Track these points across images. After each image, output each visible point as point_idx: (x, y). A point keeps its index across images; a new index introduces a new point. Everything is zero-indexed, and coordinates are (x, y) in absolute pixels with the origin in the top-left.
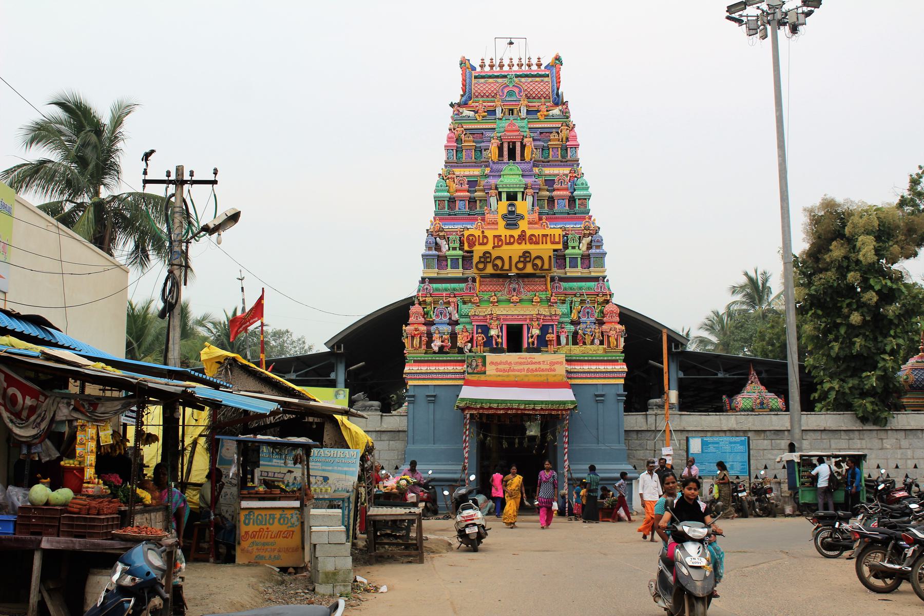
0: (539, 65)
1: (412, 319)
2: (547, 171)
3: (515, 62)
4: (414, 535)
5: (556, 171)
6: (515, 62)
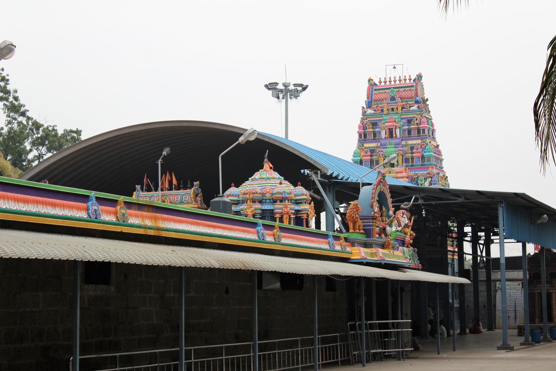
0: (410, 80)
2: (410, 142)
3: (397, 79)
4: (495, 252)
5: (415, 142)
6: (397, 79)
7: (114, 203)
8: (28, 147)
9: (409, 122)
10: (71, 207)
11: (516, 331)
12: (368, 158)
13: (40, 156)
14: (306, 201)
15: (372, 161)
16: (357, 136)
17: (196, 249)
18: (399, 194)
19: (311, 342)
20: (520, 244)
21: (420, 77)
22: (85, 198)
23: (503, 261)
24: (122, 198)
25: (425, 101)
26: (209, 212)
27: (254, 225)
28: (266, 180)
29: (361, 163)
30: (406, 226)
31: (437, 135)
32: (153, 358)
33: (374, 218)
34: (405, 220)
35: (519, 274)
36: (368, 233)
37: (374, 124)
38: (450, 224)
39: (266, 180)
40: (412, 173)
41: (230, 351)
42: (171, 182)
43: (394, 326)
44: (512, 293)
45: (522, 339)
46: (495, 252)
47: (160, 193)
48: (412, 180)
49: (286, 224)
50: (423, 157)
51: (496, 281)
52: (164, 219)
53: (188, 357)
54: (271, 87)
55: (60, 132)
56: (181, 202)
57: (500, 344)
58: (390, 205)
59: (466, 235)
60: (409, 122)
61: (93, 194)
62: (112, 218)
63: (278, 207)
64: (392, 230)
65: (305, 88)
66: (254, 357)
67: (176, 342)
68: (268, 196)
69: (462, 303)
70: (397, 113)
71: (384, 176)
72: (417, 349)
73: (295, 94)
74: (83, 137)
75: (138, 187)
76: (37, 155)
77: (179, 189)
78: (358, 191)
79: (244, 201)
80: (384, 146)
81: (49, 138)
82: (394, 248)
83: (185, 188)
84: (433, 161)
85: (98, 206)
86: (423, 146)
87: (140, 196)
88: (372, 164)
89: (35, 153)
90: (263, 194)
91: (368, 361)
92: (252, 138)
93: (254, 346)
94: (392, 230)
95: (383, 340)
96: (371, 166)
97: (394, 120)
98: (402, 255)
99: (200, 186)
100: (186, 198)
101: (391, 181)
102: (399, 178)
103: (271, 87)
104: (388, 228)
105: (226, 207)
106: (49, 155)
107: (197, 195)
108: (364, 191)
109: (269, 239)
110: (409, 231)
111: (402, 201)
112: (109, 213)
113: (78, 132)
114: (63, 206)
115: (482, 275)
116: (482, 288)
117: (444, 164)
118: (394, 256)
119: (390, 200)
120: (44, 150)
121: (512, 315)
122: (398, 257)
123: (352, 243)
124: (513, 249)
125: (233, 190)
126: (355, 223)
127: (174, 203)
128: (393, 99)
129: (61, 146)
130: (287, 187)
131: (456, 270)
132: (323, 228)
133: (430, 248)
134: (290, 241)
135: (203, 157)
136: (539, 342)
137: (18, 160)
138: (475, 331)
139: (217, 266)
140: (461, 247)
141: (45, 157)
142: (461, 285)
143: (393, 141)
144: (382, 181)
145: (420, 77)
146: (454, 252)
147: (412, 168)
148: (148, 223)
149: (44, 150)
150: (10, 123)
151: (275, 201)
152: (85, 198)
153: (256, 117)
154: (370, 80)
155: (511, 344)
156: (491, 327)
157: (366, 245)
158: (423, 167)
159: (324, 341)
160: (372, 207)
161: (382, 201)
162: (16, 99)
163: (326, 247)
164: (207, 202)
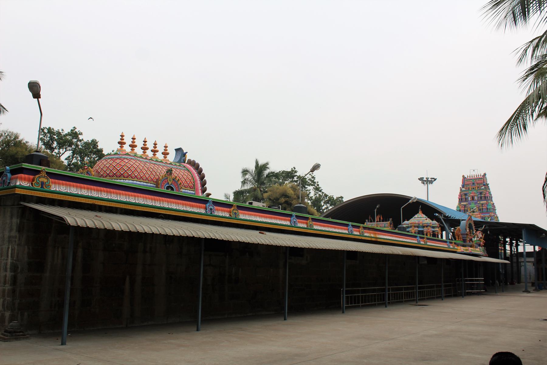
4: (521, 249)
7: (359, 227)
8: (323, 204)
9: (481, 193)
10: (342, 229)
11: (530, 284)
12: (463, 209)
13: (327, 208)
14: (437, 227)
15: (465, 210)
16: (458, 200)
17: (267, 233)
18: (478, 224)
19: (440, 286)
20: (532, 247)
21: (485, 174)
22: (347, 225)
23: (525, 254)
24: (362, 225)
25: (487, 185)
26: (396, 231)
27: (416, 237)
28: (420, 218)
29: (460, 211)
30: (481, 238)
31: (493, 199)
32: (374, 291)
33: (467, 234)
34: (480, 236)
35: (532, 259)
36: (464, 241)
37: (466, 195)
38: (500, 237)
39: (420, 218)
40: (482, 215)
41: (406, 289)
42: (380, 218)
43: (476, 281)
44: (529, 268)
45: (534, 288)
46: (521, 249)
47: (376, 223)
48: (482, 218)
49: (428, 237)
50: (487, 209)
51: (521, 262)
52: (379, 234)
53: (389, 291)
54: (421, 179)
55: (335, 198)
56: (384, 227)
57: (524, 290)
58: (474, 229)
59: (507, 242)
60: (481, 193)
61: (350, 223)
62: (358, 233)
63: (425, 229)
64: (475, 239)
65: (435, 180)
66: (416, 292)
67: (384, 284)
68: (421, 225)
69: (506, 271)
70: (475, 190)
71: (471, 217)
72: (486, 291)
73: (431, 182)
74: (345, 200)
75: (367, 220)
76: (326, 207)
77: (383, 221)
78: (459, 223)
79: (411, 227)
80: (470, 204)
81: (331, 201)
82: (476, 247)
83: (386, 221)
84: (492, 210)
85: (47, 179)
86: (487, 204)
87: (368, 224)
88: (465, 211)
89: (325, 206)
90: (419, 224)
91: (465, 295)
92: (415, 201)
93: (416, 287)
94: (475, 239)
95: (471, 287)
96: (465, 212)
97: (475, 193)
98: (479, 250)
99: (392, 220)
100: (386, 225)
101: (474, 219)
102: (477, 218)
103: (421, 179)
104: (473, 239)
105: (404, 229)
106: (331, 207)
107: (391, 224)
108: (462, 222)
109: (422, 243)
110: (482, 240)
111: (479, 227)
112: (357, 231)
113: (342, 197)
114: (338, 228)
115: (515, 259)
116: (515, 265)
117: (497, 211)
118: (476, 251)
119: (474, 227)
120: (329, 205)
121: (528, 277)
122: (478, 251)
123: (458, 245)
124: (529, 248)
125: (406, 222)
126: (458, 236)
127: (102, 176)
128: (473, 184)
129: (335, 204)
130: (429, 221)
131: (503, 257)
132: (444, 238)
133: (492, 247)
134: (430, 244)
135: (392, 209)
136: (542, 289)
137: (319, 208)
138: (512, 283)
139: (401, 253)
140: (505, 247)
141: (329, 208)
142: (505, 264)
143: (474, 202)
144: (470, 219)
145: (485, 174)
146: (501, 249)
147: (482, 213)
148: (372, 235)
149: (329, 205)
150: (315, 194)
151: (423, 227)
152: (291, 216)
153: (416, 192)
154: (463, 176)
155: (529, 290)
156: (519, 282)
157: (463, 246)
158: (487, 213)
159: (445, 286)
160: (466, 229)
161: (470, 227)
162: (318, 185)
163: (446, 246)
164: (395, 227)
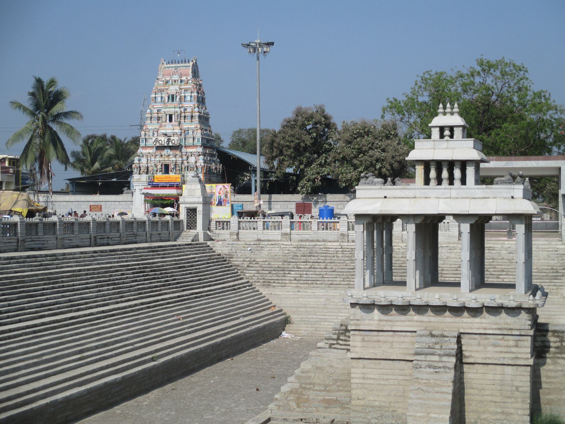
1: (135, 162)
